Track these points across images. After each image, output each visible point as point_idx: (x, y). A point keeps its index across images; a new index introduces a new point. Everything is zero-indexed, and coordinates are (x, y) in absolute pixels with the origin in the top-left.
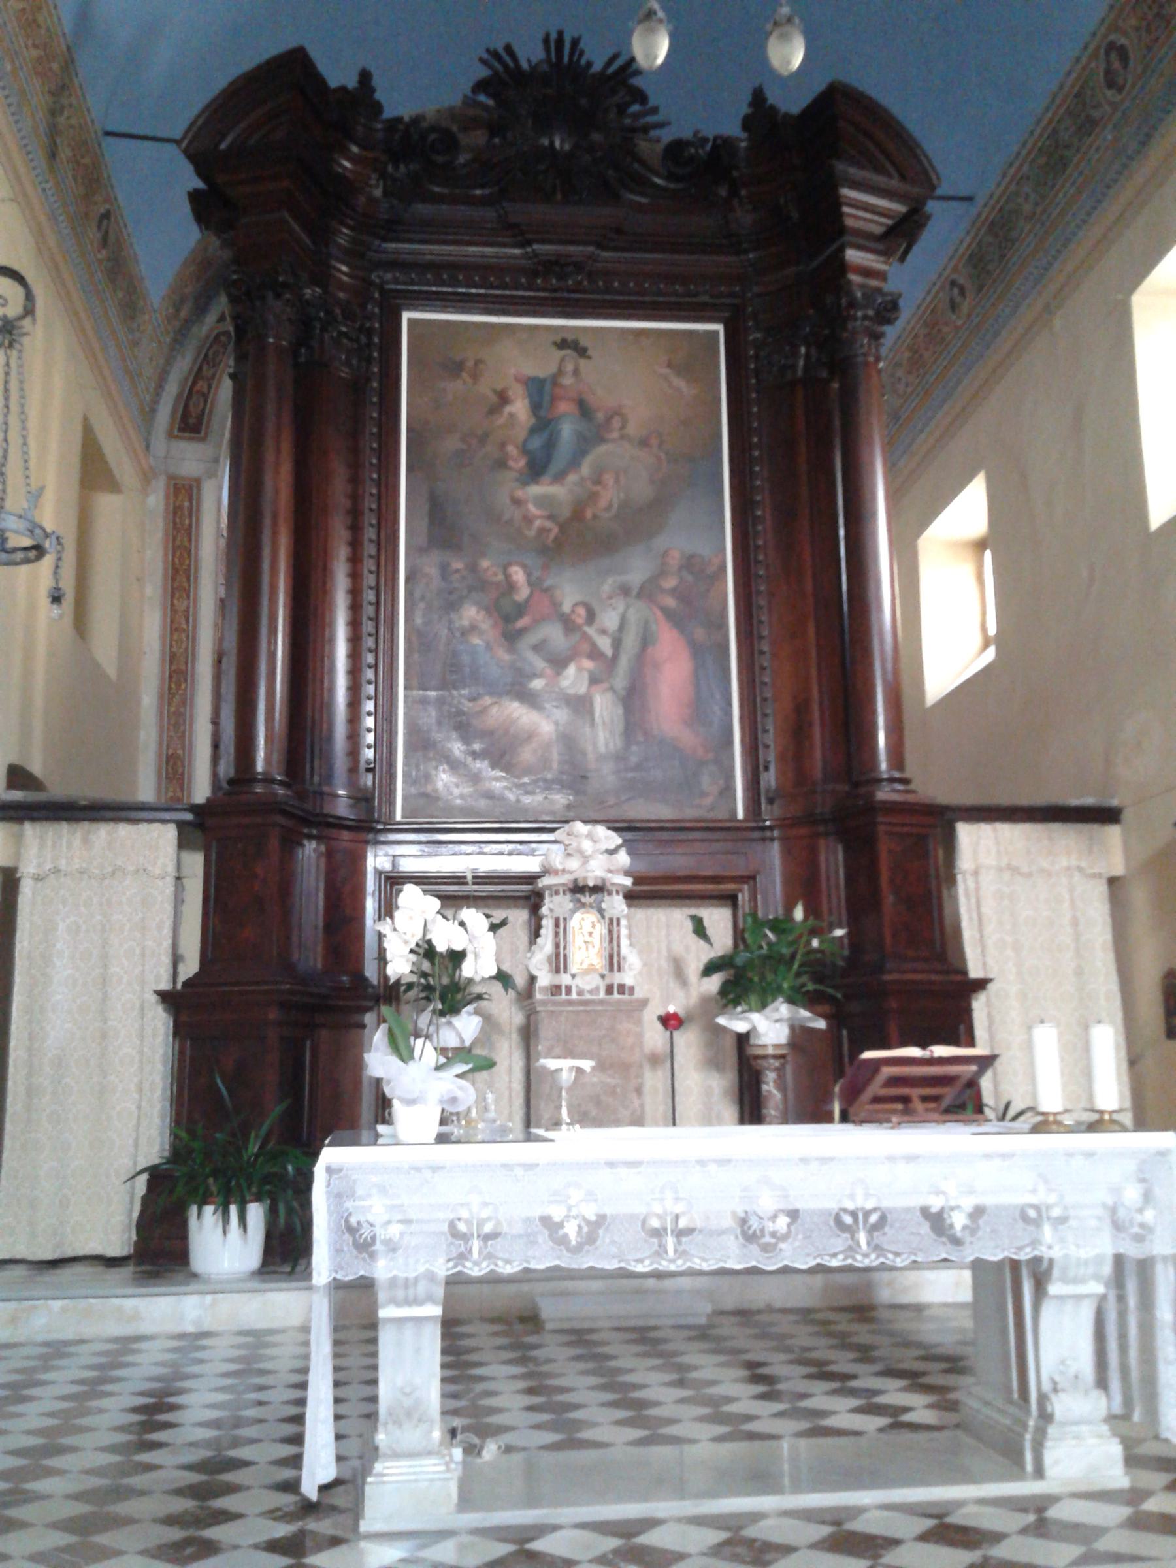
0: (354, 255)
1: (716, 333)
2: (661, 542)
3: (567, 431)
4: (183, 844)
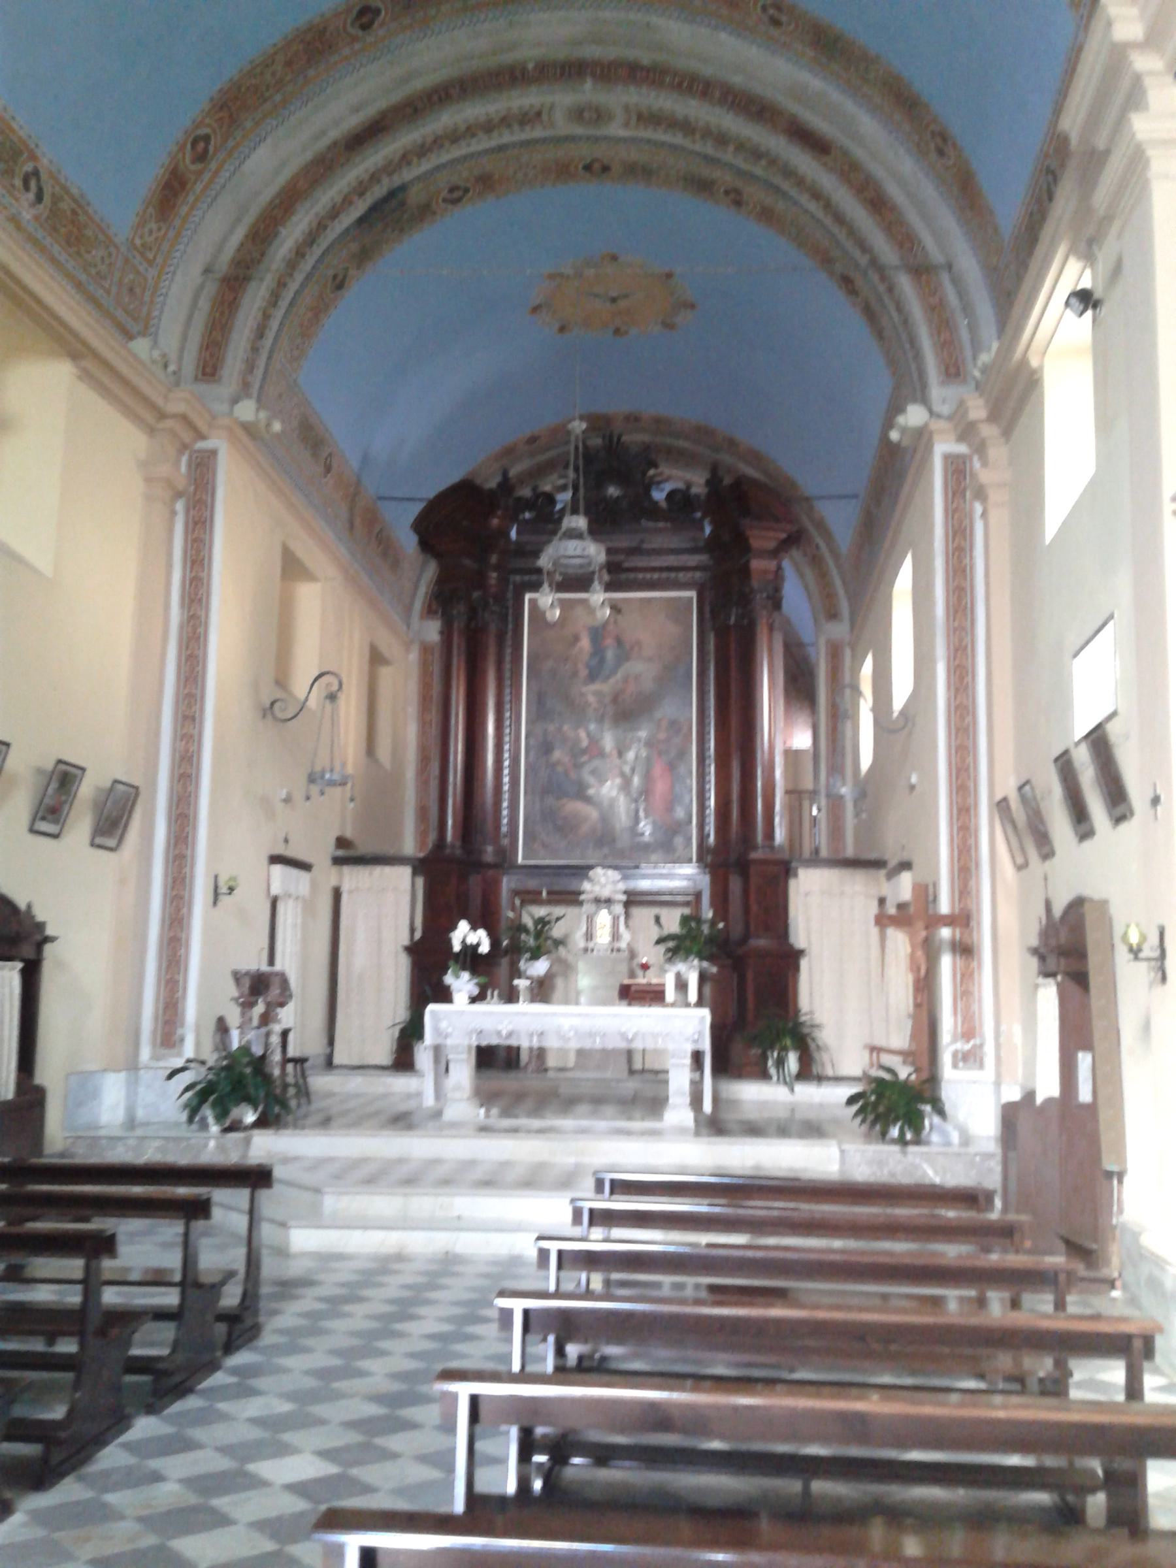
0: (498, 567)
1: (692, 598)
2: (658, 714)
3: (610, 655)
4: (415, 873)
